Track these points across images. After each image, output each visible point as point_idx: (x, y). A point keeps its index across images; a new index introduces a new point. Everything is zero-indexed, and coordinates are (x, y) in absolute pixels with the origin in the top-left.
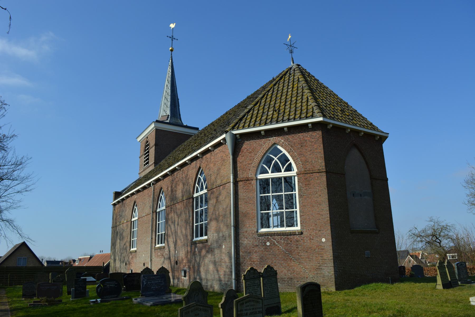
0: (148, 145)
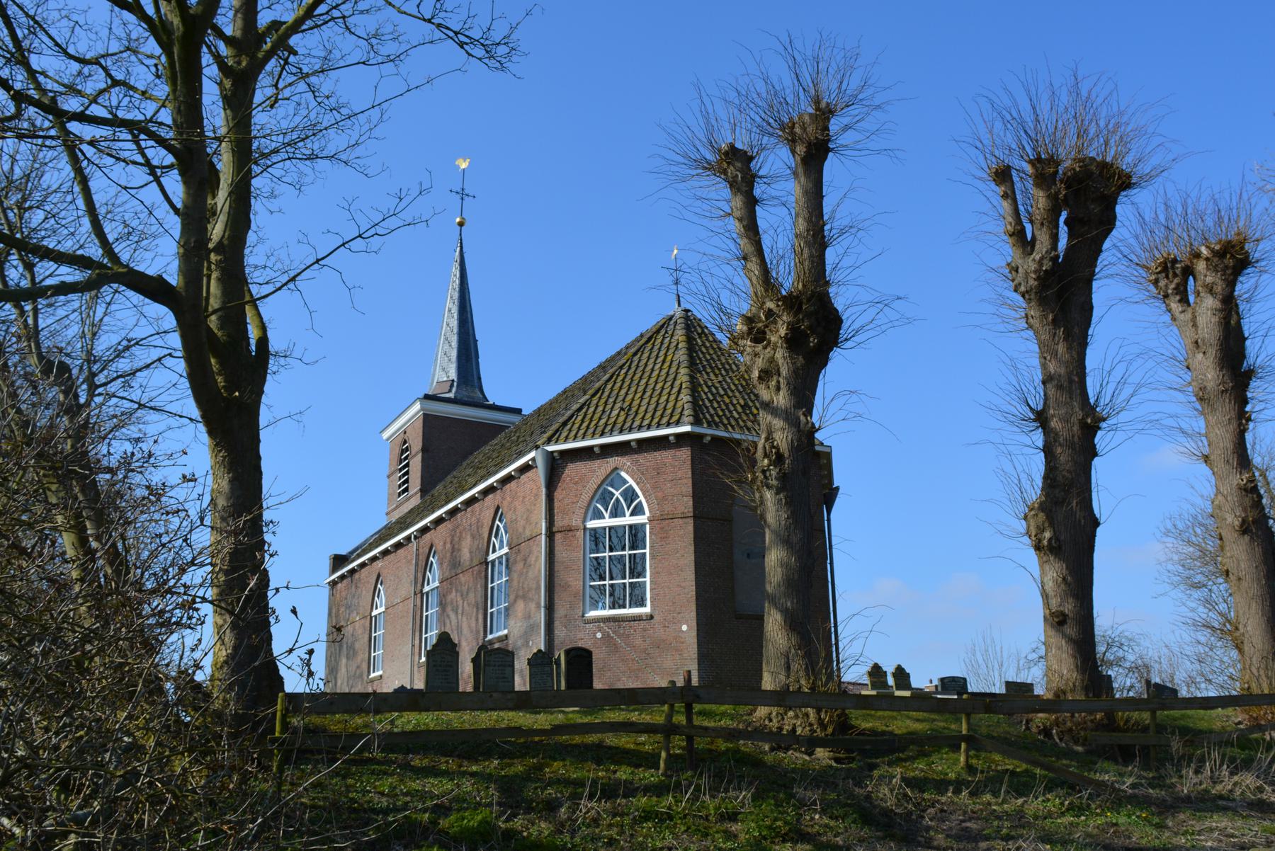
0: (407, 449)
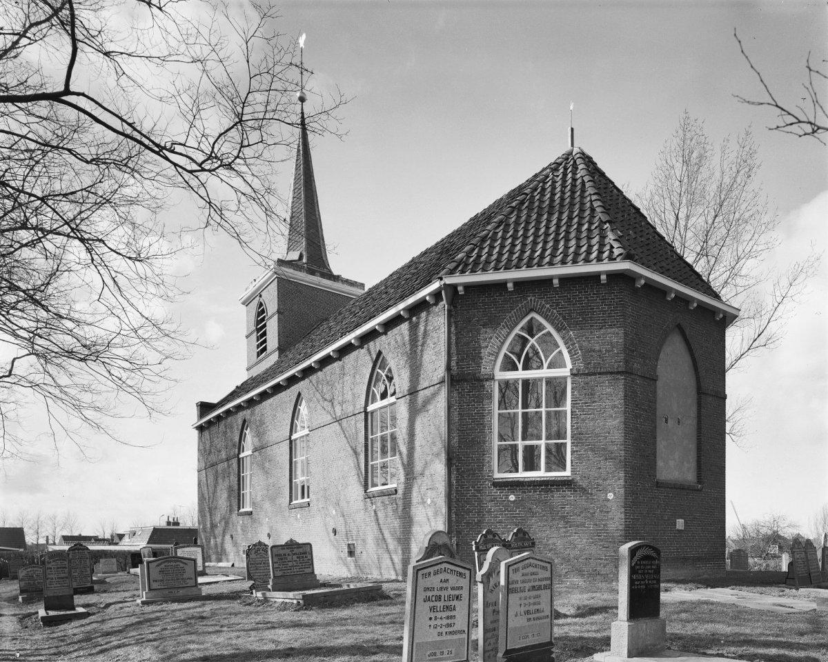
0: (263, 311)
